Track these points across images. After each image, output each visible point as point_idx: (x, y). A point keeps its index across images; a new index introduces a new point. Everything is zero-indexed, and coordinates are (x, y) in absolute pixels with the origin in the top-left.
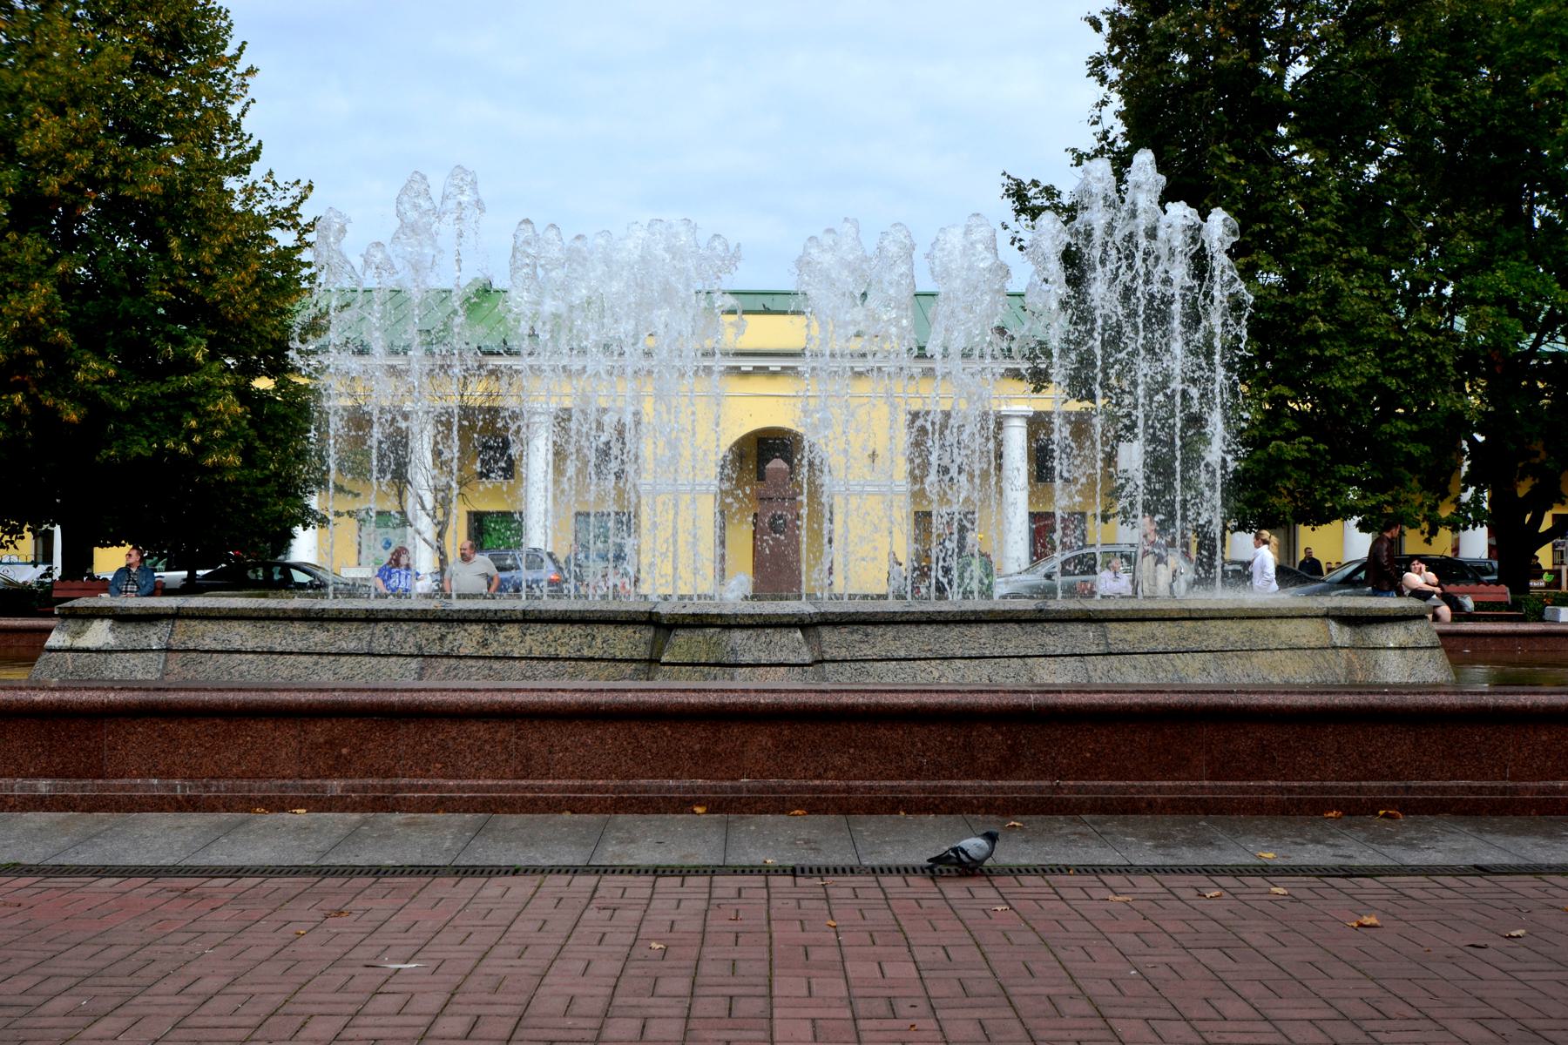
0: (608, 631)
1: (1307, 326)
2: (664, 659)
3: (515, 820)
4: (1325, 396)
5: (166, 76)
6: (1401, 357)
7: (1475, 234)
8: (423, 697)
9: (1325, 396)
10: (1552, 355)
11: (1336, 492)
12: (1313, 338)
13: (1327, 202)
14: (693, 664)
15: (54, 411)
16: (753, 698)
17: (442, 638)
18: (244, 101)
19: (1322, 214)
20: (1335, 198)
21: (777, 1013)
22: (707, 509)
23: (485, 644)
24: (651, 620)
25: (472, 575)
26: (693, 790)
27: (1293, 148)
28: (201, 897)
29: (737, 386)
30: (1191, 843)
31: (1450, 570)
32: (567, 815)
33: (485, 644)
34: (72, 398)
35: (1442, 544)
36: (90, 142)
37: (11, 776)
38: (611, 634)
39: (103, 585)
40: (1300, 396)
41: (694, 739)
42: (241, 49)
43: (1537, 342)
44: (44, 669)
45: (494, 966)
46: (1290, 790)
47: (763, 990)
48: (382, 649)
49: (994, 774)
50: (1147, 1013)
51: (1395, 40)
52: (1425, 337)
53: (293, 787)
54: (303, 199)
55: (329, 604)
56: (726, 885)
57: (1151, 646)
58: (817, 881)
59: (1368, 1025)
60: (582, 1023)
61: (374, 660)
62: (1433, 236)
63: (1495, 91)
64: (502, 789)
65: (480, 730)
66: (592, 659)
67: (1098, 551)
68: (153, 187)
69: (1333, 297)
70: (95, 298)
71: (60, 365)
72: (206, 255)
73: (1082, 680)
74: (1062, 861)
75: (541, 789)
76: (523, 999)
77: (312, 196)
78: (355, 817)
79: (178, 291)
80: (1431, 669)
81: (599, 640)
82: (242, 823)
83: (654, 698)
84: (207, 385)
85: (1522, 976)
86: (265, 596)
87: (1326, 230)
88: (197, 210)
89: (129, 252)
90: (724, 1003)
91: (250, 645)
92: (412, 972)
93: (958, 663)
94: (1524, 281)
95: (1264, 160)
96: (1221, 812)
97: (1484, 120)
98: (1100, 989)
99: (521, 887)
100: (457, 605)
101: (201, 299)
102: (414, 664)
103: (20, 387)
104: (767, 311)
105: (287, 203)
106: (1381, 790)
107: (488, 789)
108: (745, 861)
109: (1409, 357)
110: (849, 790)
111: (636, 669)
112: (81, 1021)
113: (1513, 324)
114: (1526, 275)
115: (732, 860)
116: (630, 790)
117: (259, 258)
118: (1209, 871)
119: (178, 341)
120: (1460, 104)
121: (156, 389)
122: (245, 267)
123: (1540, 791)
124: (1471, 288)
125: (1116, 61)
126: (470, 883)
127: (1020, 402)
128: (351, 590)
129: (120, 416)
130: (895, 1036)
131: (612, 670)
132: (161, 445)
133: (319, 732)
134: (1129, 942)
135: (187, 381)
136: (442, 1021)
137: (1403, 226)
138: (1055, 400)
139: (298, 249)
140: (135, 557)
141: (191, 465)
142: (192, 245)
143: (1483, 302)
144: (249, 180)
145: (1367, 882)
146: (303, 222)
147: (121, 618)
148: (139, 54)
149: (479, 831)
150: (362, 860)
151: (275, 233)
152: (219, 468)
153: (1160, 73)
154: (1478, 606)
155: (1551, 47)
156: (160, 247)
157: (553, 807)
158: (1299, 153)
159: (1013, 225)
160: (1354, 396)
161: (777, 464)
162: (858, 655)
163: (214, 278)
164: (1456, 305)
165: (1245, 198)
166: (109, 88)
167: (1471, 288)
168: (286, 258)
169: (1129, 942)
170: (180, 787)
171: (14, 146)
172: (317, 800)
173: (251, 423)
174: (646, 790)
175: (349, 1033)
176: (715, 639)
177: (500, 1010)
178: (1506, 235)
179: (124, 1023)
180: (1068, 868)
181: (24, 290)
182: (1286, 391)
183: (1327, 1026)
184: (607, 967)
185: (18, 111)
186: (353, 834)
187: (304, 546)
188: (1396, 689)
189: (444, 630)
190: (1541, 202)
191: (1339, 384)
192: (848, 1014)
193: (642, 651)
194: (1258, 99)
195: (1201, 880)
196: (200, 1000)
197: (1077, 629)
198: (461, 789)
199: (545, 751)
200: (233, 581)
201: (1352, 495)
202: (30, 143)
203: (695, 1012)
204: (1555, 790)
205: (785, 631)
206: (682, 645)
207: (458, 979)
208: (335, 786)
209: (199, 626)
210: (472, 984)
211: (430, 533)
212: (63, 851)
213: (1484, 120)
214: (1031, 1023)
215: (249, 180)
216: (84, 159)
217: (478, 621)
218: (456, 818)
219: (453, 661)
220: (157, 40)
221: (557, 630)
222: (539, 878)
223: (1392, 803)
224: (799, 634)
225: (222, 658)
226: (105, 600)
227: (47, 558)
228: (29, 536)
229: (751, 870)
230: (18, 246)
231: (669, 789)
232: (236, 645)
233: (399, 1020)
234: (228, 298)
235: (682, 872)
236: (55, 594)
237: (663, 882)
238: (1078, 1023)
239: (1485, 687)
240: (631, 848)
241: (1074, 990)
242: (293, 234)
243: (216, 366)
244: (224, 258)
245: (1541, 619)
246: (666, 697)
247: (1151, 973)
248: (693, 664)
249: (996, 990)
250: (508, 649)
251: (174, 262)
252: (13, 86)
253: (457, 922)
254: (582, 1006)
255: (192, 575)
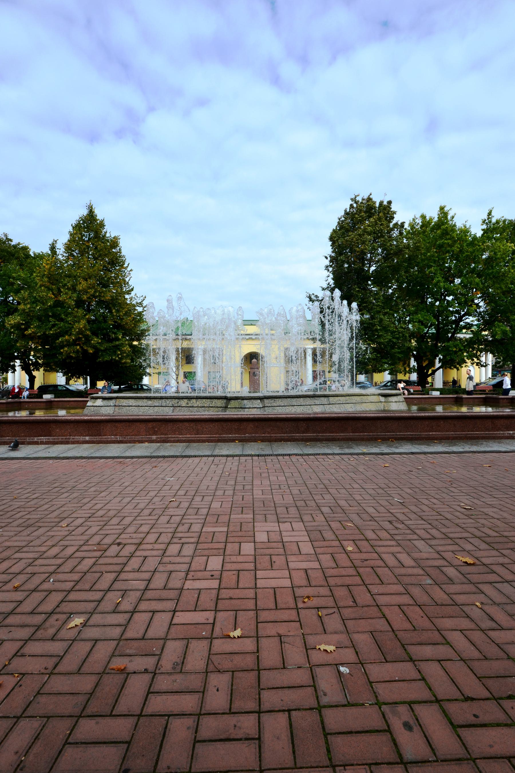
0: (216, 401)
1: (375, 328)
2: (229, 407)
3: (195, 444)
4: (379, 343)
5: (111, 271)
6: (397, 334)
7: (413, 306)
8: (174, 417)
9: (379, 343)
10: (431, 333)
11: (382, 366)
12: (377, 330)
13: (380, 299)
14: (235, 408)
15: (87, 350)
16: (249, 416)
17: (178, 402)
18: (130, 277)
19: (378, 302)
20: (382, 298)
21: (254, 489)
22: (239, 370)
23: (188, 404)
24: (225, 398)
25: (185, 388)
26: (235, 437)
27: (372, 286)
28: (124, 463)
29: (244, 342)
30: (347, 448)
31: (408, 383)
32: (207, 443)
33: (188, 404)
34: (91, 347)
35: (406, 378)
36: (93, 287)
37: (80, 436)
39: (100, 390)
40: (374, 343)
41: (235, 425)
42: (128, 265)
43: (428, 330)
44: (86, 411)
45: (191, 478)
46: (370, 435)
47: (251, 483)
48: (164, 405)
49: (303, 433)
50: (336, 487)
51: (396, 261)
52: (402, 330)
53: (144, 437)
54: (144, 300)
55: (152, 395)
56: (243, 459)
57: (339, 402)
58: (263, 458)
59: (385, 490)
60: (211, 492)
61: (162, 408)
62: (404, 307)
63: (418, 273)
64: (192, 437)
65: (187, 424)
67: (327, 379)
68: (108, 298)
69: (381, 320)
70: (96, 324)
71: (88, 340)
72: (121, 314)
73: (324, 410)
74: (319, 452)
75: (201, 437)
76: (197, 486)
78: (159, 444)
79: (115, 322)
80: (403, 407)
82: (133, 446)
83: (226, 416)
84: (122, 344)
85: (420, 478)
86: (137, 393)
87: (379, 305)
88: (119, 303)
89: (103, 313)
90: (242, 486)
91: (134, 405)
92: (172, 480)
93: (295, 407)
94: (425, 317)
95: (365, 289)
96: (354, 440)
97: (416, 279)
98: (326, 482)
99: (197, 460)
100: (181, 395)
101: (120, 323)
102: (172, 408)
103: (79, 345)
104: (252, 325)
105: (140, 301)
106: (390, 435)
107: (189, 437)
108: (247, 453)
109: (398, 334)
110: (270, 437)
112: (97, 493)
113: (422, 327)
114: (426, 315)
115: (244, 453)
116: (221, 437)
117: (134, 314)
118: (351, 454)
119: (115, 333)
120: (410, 276)
121: (111, 345)
122: (130, 316)
123: (426, 435)
124: (413, 319)
125: (331, 266)
126: (185, 459)
127: (310, 346)
128: (157, 391)
129: (102, 350)
130: (280, 493)
132: (112, 358)
133: (150, 425)
134: (333, 471)
135: (117, 343)
136: (179, 492)
137: (397, 305)
138: (318, 345)
139: (143, 312)
140: (106, 384)
141: (119, 362)
142: (118, 311)
143: (415, 322)
144: (131, 296)
145: (387, 456)
146: (144, 305)
147: (104, 399)
148: (104, 266)
149: (187, 447)
150: (160, 454)
151: (137, 308)
152: (125, 363)
153: (341, 269)
154: (414, 391)
155: (432, 262)
156: (111, 312)
157: (204, 441)
158: (373, 287)
159: (308, 305)
160: (386, 343)
161: (254, 360)
162: (273, 405)
163: (123, 319)
164: (409, 322)
165: (361, 298)
166: (98, 274)
167: (413, 319)
168: (140, 314)
169: (333, 471)
170: (119, 438)
171: (76, 288)
172: (150, 440)
173: (133, 352)
174: (224, 437)
175: (158, 495)
177: (192, 489)
178: (421, 306)
179: (107, 493)
180: (320, 454)
181: (79, 322)
182: (371, 343)
183: (376, 490)
184: (216, 479)
185: (76, 280)
186: (159, 448)
187: (146, 380)
188: (394, 411)
190: (429, 297)
191: (382, 341)
192: (270, 489)
193: (224, 405)
194: (364, 275)
195: (350, 456)
196: (124, 487)
197: (322, 399)
198: (182, 437)
199: (202, 428)
200: (129, 389)
201: (386, 366)
202: (80, 287)
203: (236, 488)
204: (430, 435)
206: (233, 404)
207: (183, 482)
208: (154, 437)
209: (122, 400)
210: (185, 483)
211: (175, 377)
212: (92, 453)
213: (416, 279)
214: (311, 490)
215: (131, 296)
216: (92, 291)
217: (186, 399)
218: (182, 444)
220: (109, 263)
221: (204, 400)
222: (200, 458)
223: (393, 438)
224: (259, 401)
225: (128, 407)
226: (100, 394)
227: (86, 383)
228: (81, 379)
229: (247, 456)
230: (77, 312)
231: (230, 437)
232: (131, 405)
233: (170, 491)
234: (127, 323)
235: (233, 456)
236: (89, 392)
237: (229, 458)
238: (321, 490)
239: (416, 411)
240: (221, 451)
241: (320, 482)
242: (142, 308)
243: (124, 339)
244: (126, 314)
245: (428, 394)
246: (229, 416)
247: (337, 478)
248: (235, 408)
249: (303, 482)
251: (114, 315)
252: (75, 274)
253: (182, 468)
254: (210, 488)
255: (120, 387)
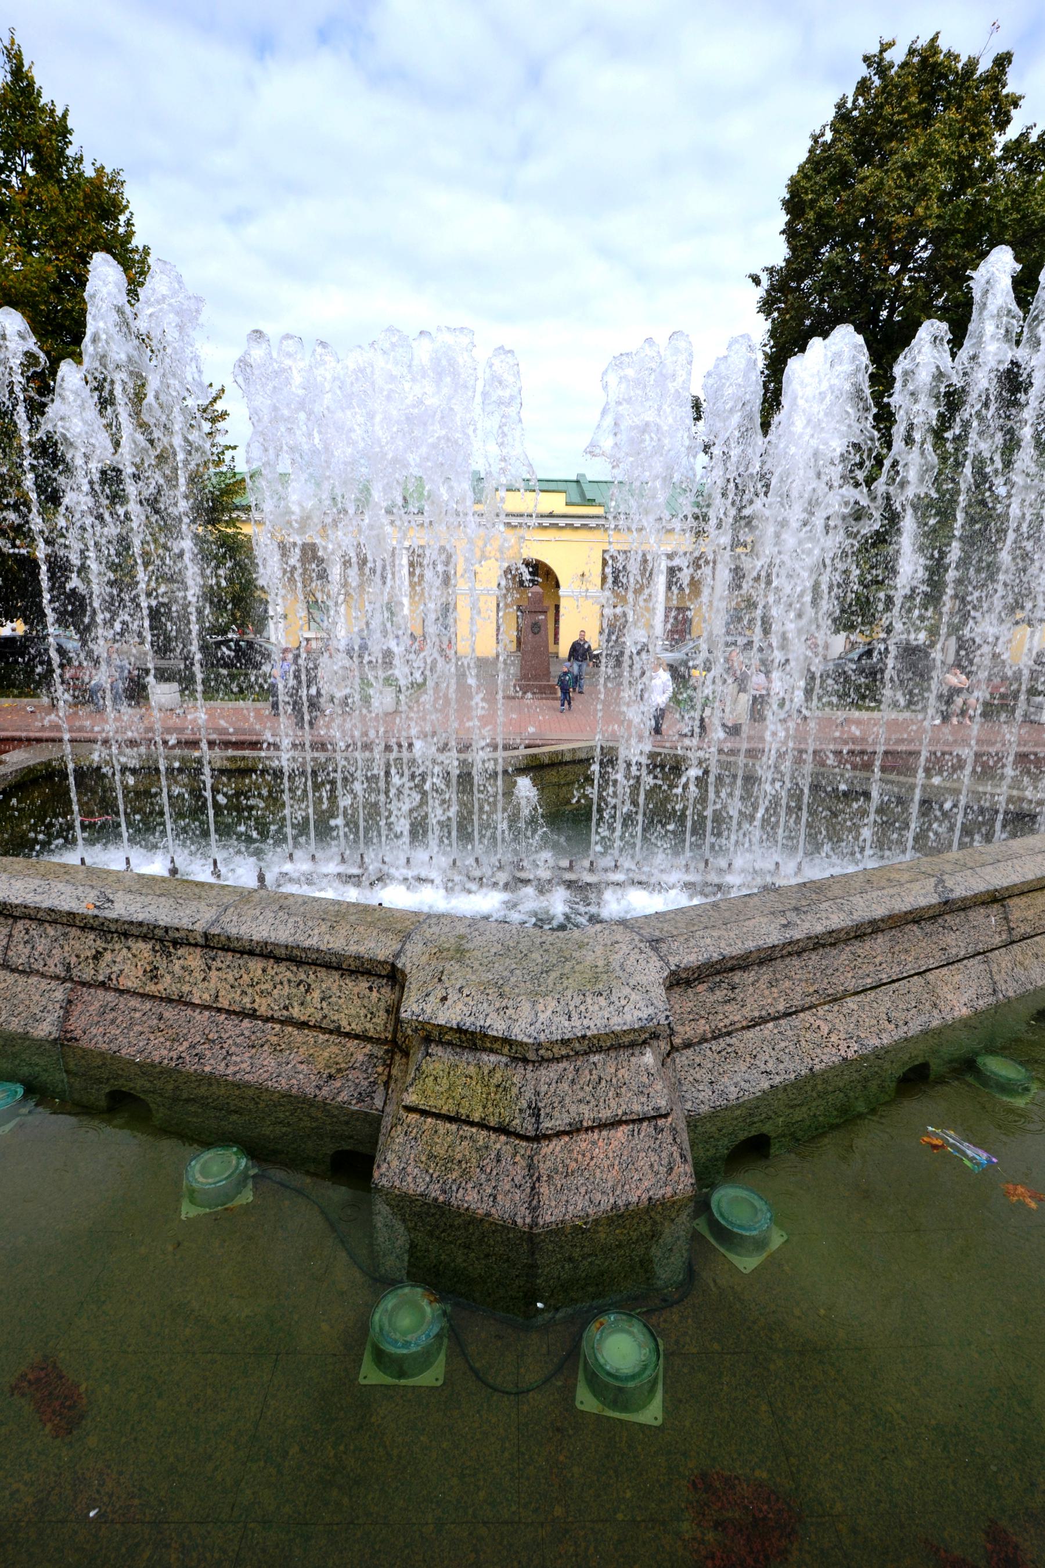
0: (331, 981)
17: (97, 956)
33: (153, 975)
38: (335, 988)
66: (303, 1025)
77: (224, 396)
81: (316, 994)
93: (851, 1003)
111: (371, 1056)
131: (335, 1049)
176: (498, 1076)
189: (100, 944)
205: (624, 1055)
219: (110, 997)
221: (256, 965)
250: (186, 988)
